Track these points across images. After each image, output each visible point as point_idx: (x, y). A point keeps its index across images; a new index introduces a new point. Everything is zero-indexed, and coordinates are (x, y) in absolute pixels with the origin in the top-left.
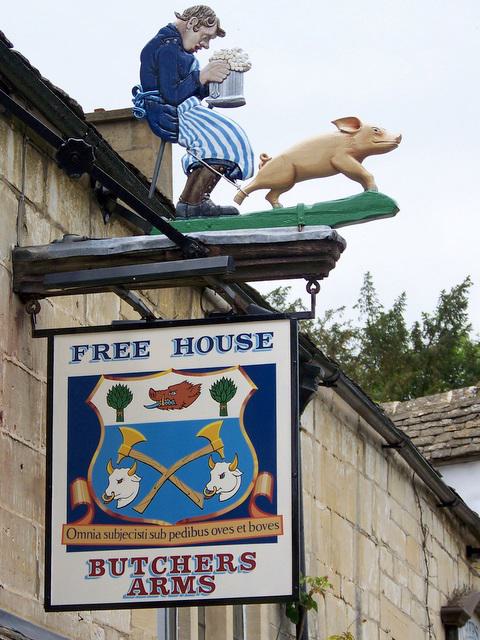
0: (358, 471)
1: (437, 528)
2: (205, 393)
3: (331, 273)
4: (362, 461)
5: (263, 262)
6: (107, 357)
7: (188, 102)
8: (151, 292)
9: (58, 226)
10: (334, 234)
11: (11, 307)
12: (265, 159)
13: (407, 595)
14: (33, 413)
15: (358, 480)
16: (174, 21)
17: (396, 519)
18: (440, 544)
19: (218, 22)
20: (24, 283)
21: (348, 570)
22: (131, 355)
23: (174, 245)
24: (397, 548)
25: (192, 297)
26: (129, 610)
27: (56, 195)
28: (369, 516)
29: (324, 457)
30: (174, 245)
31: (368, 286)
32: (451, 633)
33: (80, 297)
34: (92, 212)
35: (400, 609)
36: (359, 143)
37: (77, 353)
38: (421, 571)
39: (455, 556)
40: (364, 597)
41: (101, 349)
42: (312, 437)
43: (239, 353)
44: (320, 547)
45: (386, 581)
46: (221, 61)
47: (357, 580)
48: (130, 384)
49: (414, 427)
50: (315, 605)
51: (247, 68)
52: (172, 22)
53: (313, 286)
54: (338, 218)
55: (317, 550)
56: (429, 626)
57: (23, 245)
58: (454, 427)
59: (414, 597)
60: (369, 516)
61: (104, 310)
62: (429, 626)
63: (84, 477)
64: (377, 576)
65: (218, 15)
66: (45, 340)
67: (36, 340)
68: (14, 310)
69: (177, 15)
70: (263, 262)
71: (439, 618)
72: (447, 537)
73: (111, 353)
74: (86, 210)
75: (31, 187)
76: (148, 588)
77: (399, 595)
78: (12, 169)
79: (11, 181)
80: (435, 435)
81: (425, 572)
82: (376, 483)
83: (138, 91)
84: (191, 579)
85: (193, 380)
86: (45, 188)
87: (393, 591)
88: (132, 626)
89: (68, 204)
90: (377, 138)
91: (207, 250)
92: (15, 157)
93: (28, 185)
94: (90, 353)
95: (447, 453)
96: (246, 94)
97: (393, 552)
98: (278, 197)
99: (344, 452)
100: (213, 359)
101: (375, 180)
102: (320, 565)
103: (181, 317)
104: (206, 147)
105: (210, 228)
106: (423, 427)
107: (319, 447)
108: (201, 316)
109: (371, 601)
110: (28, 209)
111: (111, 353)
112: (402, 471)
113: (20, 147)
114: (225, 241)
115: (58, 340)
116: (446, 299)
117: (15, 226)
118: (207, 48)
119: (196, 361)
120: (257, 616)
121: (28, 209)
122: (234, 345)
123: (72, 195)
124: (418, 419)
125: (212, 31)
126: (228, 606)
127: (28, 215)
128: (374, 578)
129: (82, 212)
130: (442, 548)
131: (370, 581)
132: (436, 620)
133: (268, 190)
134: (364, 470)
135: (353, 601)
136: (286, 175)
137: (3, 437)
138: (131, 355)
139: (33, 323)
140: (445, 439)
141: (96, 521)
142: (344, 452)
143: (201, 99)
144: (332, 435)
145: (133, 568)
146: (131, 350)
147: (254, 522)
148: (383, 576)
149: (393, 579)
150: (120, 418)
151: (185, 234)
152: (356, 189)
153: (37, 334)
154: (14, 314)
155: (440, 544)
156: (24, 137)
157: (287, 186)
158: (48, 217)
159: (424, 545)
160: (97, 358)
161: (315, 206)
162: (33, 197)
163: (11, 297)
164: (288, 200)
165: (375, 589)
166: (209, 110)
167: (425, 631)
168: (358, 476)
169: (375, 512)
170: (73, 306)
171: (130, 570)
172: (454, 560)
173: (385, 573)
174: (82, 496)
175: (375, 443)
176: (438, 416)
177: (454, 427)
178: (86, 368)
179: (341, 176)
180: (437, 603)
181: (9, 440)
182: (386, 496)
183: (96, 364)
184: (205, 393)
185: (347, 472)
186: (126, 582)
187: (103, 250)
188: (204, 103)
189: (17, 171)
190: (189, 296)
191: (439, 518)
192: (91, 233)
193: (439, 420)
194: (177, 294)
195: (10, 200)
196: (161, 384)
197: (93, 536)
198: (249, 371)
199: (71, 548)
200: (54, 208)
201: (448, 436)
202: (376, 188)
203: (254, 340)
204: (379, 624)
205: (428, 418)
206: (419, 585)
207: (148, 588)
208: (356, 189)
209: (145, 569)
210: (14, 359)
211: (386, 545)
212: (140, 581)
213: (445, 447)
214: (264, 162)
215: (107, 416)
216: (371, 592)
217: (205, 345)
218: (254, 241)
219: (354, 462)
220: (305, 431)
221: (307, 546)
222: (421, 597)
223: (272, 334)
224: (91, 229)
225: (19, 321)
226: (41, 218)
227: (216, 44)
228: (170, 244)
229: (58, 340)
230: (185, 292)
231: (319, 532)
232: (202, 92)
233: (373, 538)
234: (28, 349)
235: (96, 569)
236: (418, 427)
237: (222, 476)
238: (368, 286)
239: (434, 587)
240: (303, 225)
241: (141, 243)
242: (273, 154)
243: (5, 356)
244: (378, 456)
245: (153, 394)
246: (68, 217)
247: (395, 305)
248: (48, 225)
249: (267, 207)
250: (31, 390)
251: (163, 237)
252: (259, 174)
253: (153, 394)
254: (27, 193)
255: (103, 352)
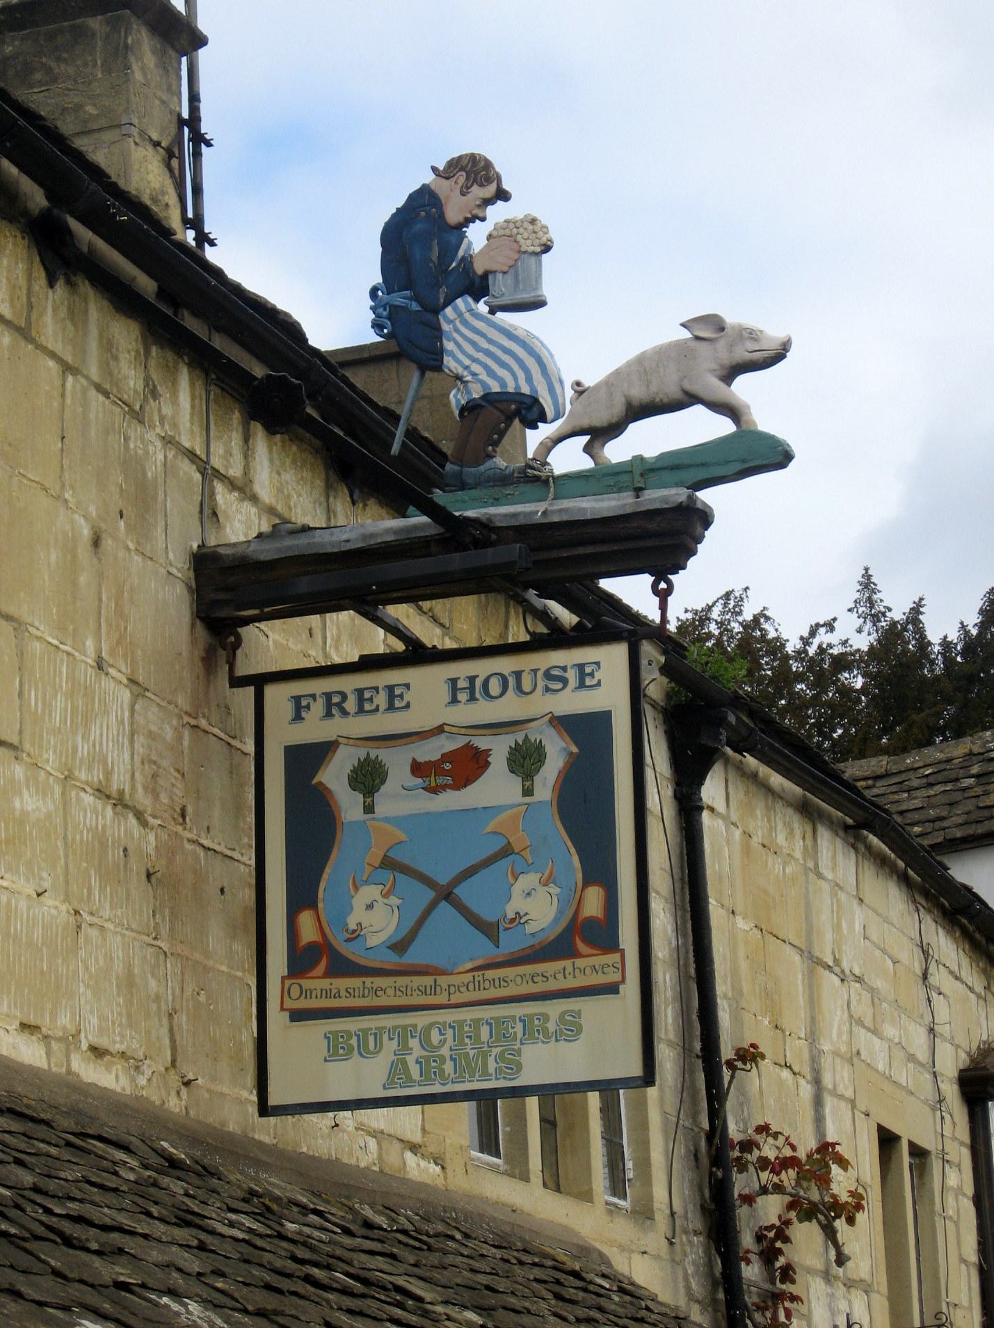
0: (806, 869)
1: (946, 947)
2: (499, 761)
3: (692, 562)
4: (812, 852)
5: (581, 551)
6: (344, 713)
7: (456, 309)
8: (438, 605)
9: (271, 511)
10: (692, 499)
11: (194, 641)
12: (578, 387)
13: (899, 1055)
14: (238, 809)
15: (807, 882)
16: (428, 178)
17: (874, 937)
18: (951, 972)
19: (499, 179)
20: (215, 604)
21: (796, 1021)
22: (382, 708)
23: (442, 530)
24: (879, 983)
25: (507, 612)
26: (419, 1107)
27: (266, 463)
28: (829, 937)
29: (747, 850)
30: (442, 530)
31: (867, 584)
32: (978, 1109)
33: (314, 620)
34: (329, 487)
35: (889, 1078)
36: (724, 354)
37: (299, 708)
38: (922, 1016)
39: (979, 988)
40: (826, 1062)
41: (336, 699)
42: (725, 818)
43: (548, 696)
44: (746, 988)
45: (862, 1035)
46: (506, 234)
47: (813, 1037)
48: (384, 754)
49: (918, 793)
50: (979, 1048)
51: (547, 248)
52: (427, 182)
53: (663, 585)
54: (702, 474)
55: (741, 993)
56: (940, 1101)
57: (212, 542)
58: (979, 790)
59: (911, 1058)
60: (829, 937)
61: (356, 638)
62: (940, 1101)
63: (313, 905)
64: (846, 1028)
65: (499, 167)
66: (251, 690)
67: (235, 690)
68: (201, 645)
69: (434, 169)
70: (581, 551)
71: (956, 1087)
72: (965, 962)
73: (351, 705)
74: (319, 483)
75: (221, 451)
76: (415, 1071)
77: (885, 1054)
78: (188, 425)
79: (187, 445)
80: (951, 804)
81: (928, 1018)
82: (837, 885)
83: (380, 293)
84: (485, 1056)
85: (482, 743)
86: (247, 454)
87: (875, 1051)
88: (423, 1130)
89: (289, 476)
90: (751, 346)
91: (494, 537)
92: (193, 407)
93: (217, 449)
94: (318, 707)
95: (970, 830)
96: (548, 289)
97: (872, 990)
98: (604, 445)
99: (781, 839)
100: (508, 707)
101: (753, 411)
102: (747, 1017)
103: (489, 641)
104: (483, 376)
105: (496, 501)
106: (932, 792)
107: (737, 833)
108: (524, 637)
109: (838, 1068)
110: (219, 488)
111: (351, 705)
112: (881, 862)
113: (199, 384)
114: (521, 521)
115: (271, 691)
116: (727, 592)
117: (197, 516)
118: (483, 219)
119: (485, 712)
120: (520, 1119)
121: (219, 488)
122: (541, 684)
123: (294, 462)
124: (924, 781)
125: (491, 190)
126: (590, 1094)
127: (219, 498)
128: (840, 1034)
129: (312, 488)
130: (957, 978)
131: (834, 1036)
132: (951, 1091)
133: (587, 438)
134: (816, 866)
135: (806, 1070)
136: (618, 410)
137: (189, 847)
138: (382, 708)
139: (232, 666)
140: (966, 809)
141: (330, 973)
142: (781, 839)
143: (477, 300)
144: (758, 813)
145: (395, 1042)
146: (381, 699)
147: (580, 962)
148: (856, 1029)
149: (875, 1032)
150: (369, 809)
151: (457, 514)
152: (723, 427)
153: (237, 682)
154: (199, 652)
155: (951, 972)
156: (207, 375)
157: (614, 430)
158: (254, 499)
159: (925, 976)
160: (329, 714)
161: (663, 456)
162: (227, 468)
163: (193, 626)
164: (618, 451)
165: (843, 1049)
166: (490, 316)
167: (933, 1109)
168: (806, 875)
169: (837, 928)
170: (305, 635)
171: (391, 1046)
172: (979, 996)
173: (860, 1023)
174: (308, 931)
175: (832, 825)
176: (953, 775)
177: (979, 790)
178: (314, 729)
179: (699, 409)
180: (950, 1063)
181: (201, 853)
182: (855, 902)
183: (328, 723)
184: (499, 761)
185: (788, 870)
186: (398, 1070)
187: (332, 544)
188: (482, 307)
189: (196, 429)
190: (503, 609)
191: (949, 932)
192: (329, 519)
193: (957, 780)
194: (483, 608)
195: (185, 473)
196: (430, 751)
197: (327, 994)
198: (569, 724)
199: (298, 1016)
200: (264, 480)
201: (970, 806)
202: (754, 423)
203: (572, 675)
204: (853, 1103)
205: (940, 777)
206: (918, 1041)
207: (415, 1071)
208: (723, 427)
209: (414, 1043)
210: (203, 723)
211: (859, 979)
212: (404, 1063)
213: (966, 823)
214: (581, 393)
215: (349, 804)
216: (836, 1053)
217: (495, 687)
218: (565, 518)
219: (798, 854)
220: (712, 809)
221: (722, 987)
222: (923, 1056)
223: (598, 664)
224: (329, 512)
225: (209, 662)
226: (242, 500)
227: (497, 213)
228: (433, 529)
229: (271, 691)
230: (496, 602)
231: (743, 965)
232: (478, 287)
233: (837, 969)
234: (227, 707)
235: (337, 1049)
236: (924, 793)
237: (370, 907)
238: (867, 584)
239: (945, 1039)
240: (641, 489)
241: (387, 531)
242: (589, 382)
243: (186, 719)
244: (839, 843)
245: (418, 769)
246: (289, 497)
247: (912, 609)
248: (254, 510)
249: (587, 463)
250: (233, 771)
251: (424, 519)
252: (571, 411)
253: (418, 769)
254: (216, 462)
255: (339, 705)
